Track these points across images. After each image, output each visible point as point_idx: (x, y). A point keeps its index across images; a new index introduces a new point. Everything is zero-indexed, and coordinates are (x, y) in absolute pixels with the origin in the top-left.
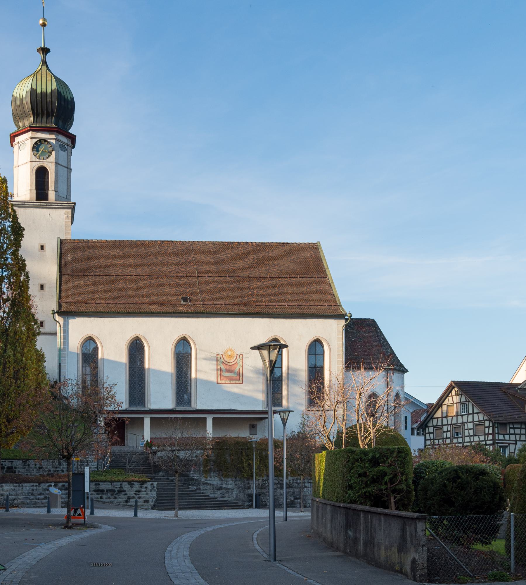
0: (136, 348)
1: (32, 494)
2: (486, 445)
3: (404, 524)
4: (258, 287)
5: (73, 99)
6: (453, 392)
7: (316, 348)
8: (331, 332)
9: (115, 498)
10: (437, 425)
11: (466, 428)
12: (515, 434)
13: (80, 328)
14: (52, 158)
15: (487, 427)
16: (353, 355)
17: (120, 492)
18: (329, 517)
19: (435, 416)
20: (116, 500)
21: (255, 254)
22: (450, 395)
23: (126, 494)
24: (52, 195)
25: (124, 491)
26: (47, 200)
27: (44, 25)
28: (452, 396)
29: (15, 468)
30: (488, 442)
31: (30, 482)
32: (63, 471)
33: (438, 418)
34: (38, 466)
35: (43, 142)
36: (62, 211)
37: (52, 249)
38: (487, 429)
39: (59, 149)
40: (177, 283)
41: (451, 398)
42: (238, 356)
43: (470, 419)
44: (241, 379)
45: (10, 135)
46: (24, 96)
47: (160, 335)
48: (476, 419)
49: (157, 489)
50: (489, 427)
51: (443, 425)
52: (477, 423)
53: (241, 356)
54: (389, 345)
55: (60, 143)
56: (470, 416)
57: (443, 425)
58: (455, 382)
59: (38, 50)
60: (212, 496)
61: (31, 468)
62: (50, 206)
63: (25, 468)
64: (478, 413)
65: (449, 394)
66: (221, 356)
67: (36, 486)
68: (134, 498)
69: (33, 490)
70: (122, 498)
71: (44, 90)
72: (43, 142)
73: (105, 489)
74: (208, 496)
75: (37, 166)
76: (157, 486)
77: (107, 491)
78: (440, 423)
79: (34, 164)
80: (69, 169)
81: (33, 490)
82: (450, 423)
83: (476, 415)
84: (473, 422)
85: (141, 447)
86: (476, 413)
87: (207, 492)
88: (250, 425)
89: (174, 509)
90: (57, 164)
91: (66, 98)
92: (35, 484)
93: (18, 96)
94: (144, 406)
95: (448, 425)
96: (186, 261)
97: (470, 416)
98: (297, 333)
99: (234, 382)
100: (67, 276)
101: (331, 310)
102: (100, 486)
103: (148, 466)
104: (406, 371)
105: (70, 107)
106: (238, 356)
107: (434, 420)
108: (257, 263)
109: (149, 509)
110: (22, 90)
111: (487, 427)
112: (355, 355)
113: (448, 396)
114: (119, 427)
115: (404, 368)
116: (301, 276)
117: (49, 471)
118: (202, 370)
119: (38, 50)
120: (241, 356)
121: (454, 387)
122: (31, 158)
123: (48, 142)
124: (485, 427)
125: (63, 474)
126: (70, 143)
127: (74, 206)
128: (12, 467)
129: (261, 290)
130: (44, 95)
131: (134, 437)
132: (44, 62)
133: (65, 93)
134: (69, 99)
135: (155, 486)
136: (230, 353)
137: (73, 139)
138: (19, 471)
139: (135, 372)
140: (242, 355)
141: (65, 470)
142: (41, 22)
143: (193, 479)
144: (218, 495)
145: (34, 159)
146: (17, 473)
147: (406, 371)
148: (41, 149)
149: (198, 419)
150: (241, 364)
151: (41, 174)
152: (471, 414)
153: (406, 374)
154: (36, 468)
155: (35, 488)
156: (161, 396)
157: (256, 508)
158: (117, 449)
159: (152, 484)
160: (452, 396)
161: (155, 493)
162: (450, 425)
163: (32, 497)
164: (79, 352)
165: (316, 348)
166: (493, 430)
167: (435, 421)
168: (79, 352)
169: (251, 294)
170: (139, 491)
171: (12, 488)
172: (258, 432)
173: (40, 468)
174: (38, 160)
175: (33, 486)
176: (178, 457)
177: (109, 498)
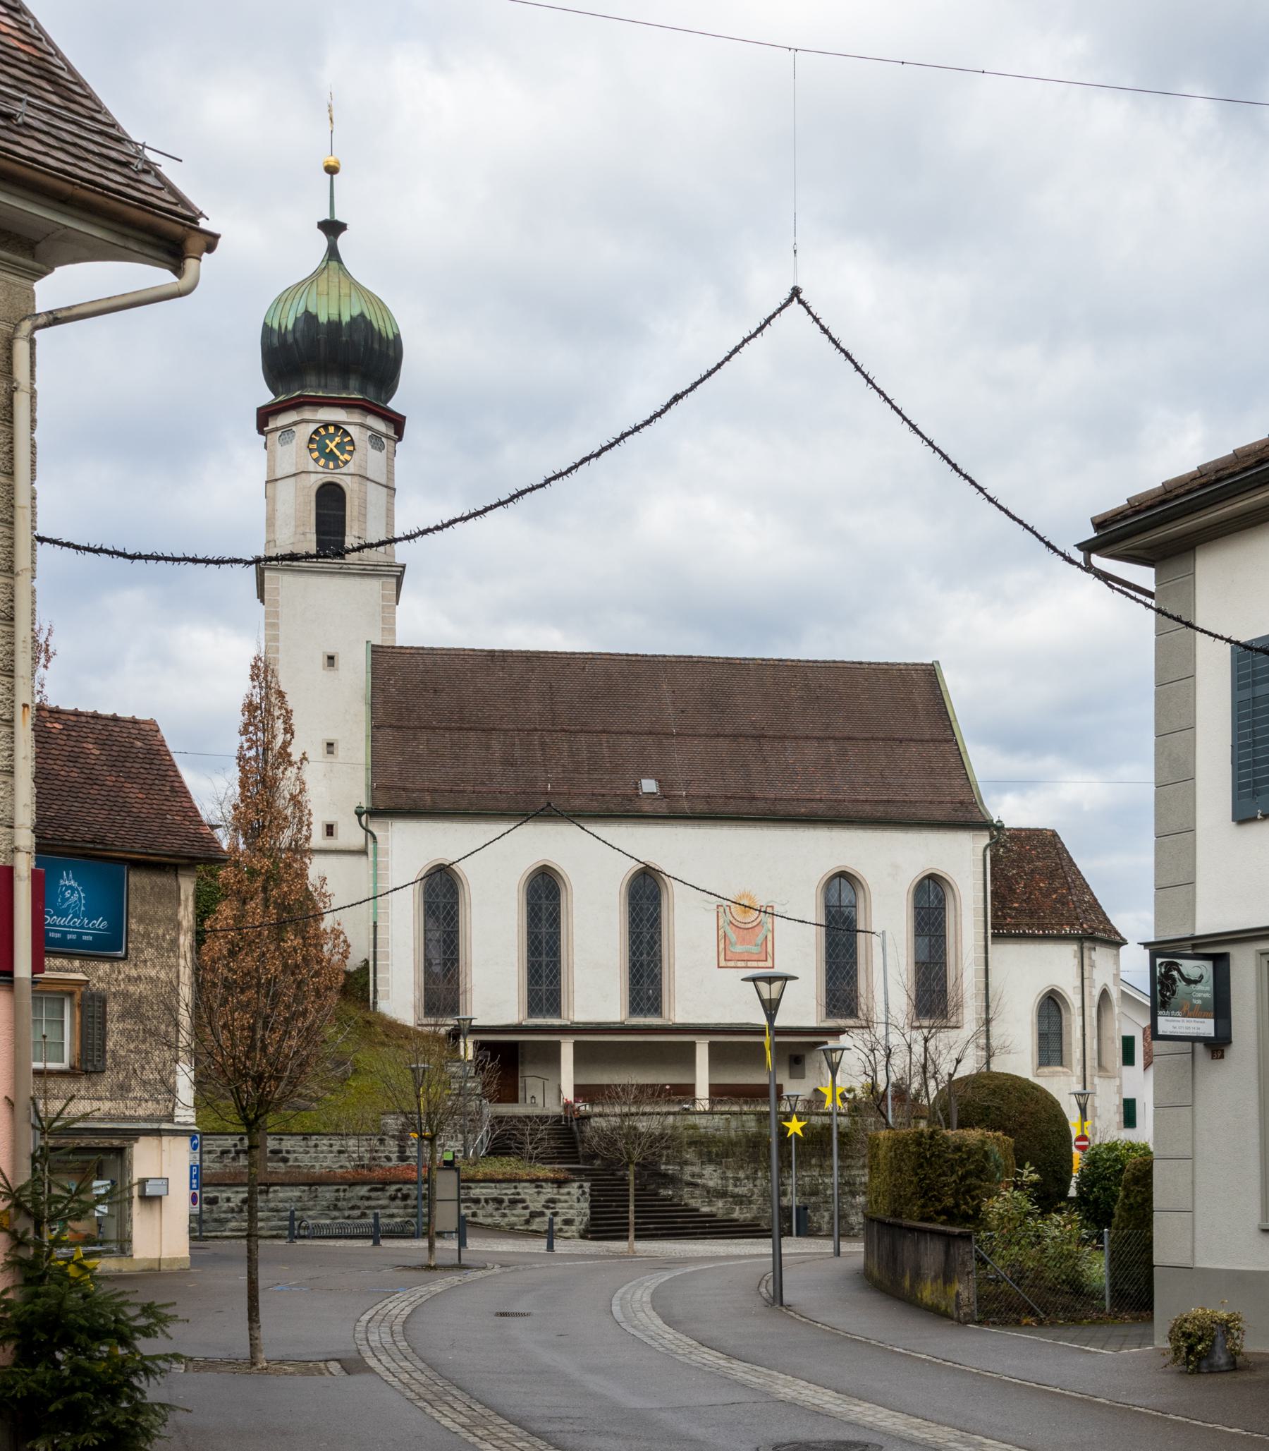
0: (544, 892)
1: (336, 1208)
3: (948, 1247)
5: (398, 336)
7: (931, 899)
8: (962, 860)
9: (504, 1215)
16: (1010, 908)
17: (513, 1202)
18: (876, 1241)
20: (506, 1219)
23: (526, 1208)
24: (778, 1039)
25: (523, 1201)
29: (288, 1152)
31: (328, 1184)
32: (389, 1159)
34: (335, 1148)
37: (355, 673)
39: (369, 447)
44: (770, 960)
46: (290, 327)
49: (591, 1195)
54: (1088, 886)
55: (370, 433)
60: (705, 1209)
61: (322, 1152)
63: (307, 1152)
67: (345, 1191)
68: (542, 1214)
69: (337, 1199)
70: (516, 1216)
71: (335, 317)
73: (482, 1197)
74: (697, 1210)
75: (320, 483)
76: (592, 1190)
77: (487, 1201)
80: (391, 489)
81: (337, 1199)
85: (553, 1109)
87: (694, 1203)
88: (791, 1056)
89: (626, 1238)
91: (384, 334)
92: (342, 1187)
93: (276, 326)
94: (559, 1016)
98: (889, 863)
101: (964, 815)
102: (472, 1192)
103: (566, 1141)
105: (391, 353)
109: (573, 1237)
112: (1015, 908)
114: (507, 1057)
115: (1119, 935)
117: (360, 1158)
118: (689, 930)
125: (390, 1164)
126: (391, 433)
127: (402, 573)
128: (280, 1152)
131: (540, 1082)
132: (333, 254)
133: (381, 323)
134: (391, 336)
135: (587, 1190)
137: (397, 423)
138: (296, 1160)
139: (540, 942)
141: (394, 1156)
143: (665, 1175)
144: (718, 1207)
146: (290, 1163)
149: (673, 1048)
153: (1123, 948)
154: (331, 1152)
155: (342, 1194)
157: (798, 1235)
158: (506, 1109)
159: (581, 1187)
161: (586, 1205)
163: (336, 1213)
170: (553, 1201)
171: (298, 1194)
172: (808, 1073)
173: (340, 1152)
174: (321, 469)
175: (338, 1191)
176: (635, 1128)
177: (491, 1215)
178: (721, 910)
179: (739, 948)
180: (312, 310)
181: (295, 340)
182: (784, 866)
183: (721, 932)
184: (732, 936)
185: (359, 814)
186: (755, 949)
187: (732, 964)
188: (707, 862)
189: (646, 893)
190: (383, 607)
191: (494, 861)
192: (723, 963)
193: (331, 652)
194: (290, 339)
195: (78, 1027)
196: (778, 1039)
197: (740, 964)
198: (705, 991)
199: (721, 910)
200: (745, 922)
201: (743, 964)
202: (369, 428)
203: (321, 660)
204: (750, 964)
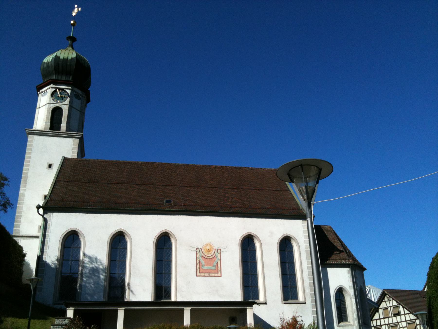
0: (118, 242)
6: (386, 299)
7: (286, 245)
8: (299, 231)
10: (377, 326)
11: (401, 326)
13: (62, 222)
15: (418, 325)
19: (374, 318)
21: (229, 173)
22: (384, 301)
24: (64, 126)
26: (60, 130)
28: (385, 301)
33: (376, 320)
36: (71, 140)
39: (74, 97)
41: (384, 303)
42: (216, 250)
43: (403, 319)
44: (219, 272)
45: (37, 87)
46: (50, 61)
47: (142, 230)
48: (408, 318)
51: (381, 325)
53: (219, 250)
56: (403, 317)
57: (381, 325)
58: (388, 290)
62: (61, 135)
64: (408, 314)
65: (383, 300)
66: (201, 250)
78: (379, 324)
79: (52, 105)
82: (387, 323)
83: (407, 316)
86: (407, 314)
95: (385, 325)
97: (403, 317)
98: (269, 231)
99: (213, 275)
100: (63, 182)
104: (365, 269)
106: (216, 250)
107: (373, 321)
111: (418, 325)
113: (382, 302)
116: (267, 189)
118: (183, 262)
119: (67, 40)
120: (219, 250)
121: (386, 294)
122: (50, 101)
123: (65, 91)
124: (417, 325)
130: (65, 60)
136: (208, 247)
140: (220, 249)
145: (52, 101)
147: (365, 269)
150: (219, 258)
151: (56, 114)
152: (403, 315)
153: (365, 272)
156: (140, 287)
160: (385, 301)
162: (388, 324)
165: (286, 245)
167: (374, 322)
174: (55, 103)
178: (198, 250)
179: (206, 268)
180: (58, 55)
181: (51, 64)
183: (198, 260)
184: (203, 262)
186: (213, 268)
187: (203, 274)
188: (192, 232)
189: (164, 243)
190: (73, 148)
192: (199, 274)
193: (50, 163)
194: (50, 64)
195: (107, 294)
196: (64, 126)
198: (187, 287)
199: (198, 250)
200: (208, 263)
202: (75, 92)
203: (46, 165)
204: (211, 274)
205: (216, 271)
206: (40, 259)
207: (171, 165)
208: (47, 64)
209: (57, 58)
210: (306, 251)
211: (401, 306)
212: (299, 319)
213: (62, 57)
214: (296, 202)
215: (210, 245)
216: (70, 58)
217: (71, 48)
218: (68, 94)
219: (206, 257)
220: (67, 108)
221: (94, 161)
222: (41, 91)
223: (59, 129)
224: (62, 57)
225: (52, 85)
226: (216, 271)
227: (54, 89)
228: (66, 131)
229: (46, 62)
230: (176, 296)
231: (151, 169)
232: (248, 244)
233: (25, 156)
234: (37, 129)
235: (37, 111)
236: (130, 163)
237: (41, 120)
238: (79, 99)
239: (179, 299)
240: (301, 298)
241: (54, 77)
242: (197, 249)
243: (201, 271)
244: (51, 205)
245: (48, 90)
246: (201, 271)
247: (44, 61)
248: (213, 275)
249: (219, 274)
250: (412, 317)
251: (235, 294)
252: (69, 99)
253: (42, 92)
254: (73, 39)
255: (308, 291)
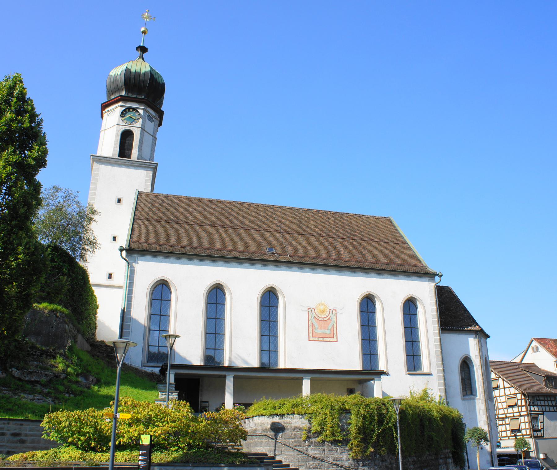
0: (216, 295)
2: (520, 416)
4: (343, 246)
7: (410, 306)
8: (425, 292)
12: (549, 406)
14: (139, 123)
27: (144, 32)
30: (522, 414)
35: (131, 110)
38: (519, 402)
39: (147, 119)
40: (260, 236)
42: (331, 311)
46: (119, 74)
48: (508, 392)
50: (521, 399)
52: (510, 396)
55: (147, 114)
59: (137, 49)
66: (313, 310)
71: (138, 70)
72: (131, 110)
80: (155, 139)
83: (507, 390)
84: (505, 395)
88: (348, 389)
90: (143, 129)
96: (268, 219)
97: (502, 391)
98: (391, 292)
99: (328, 339)
106: (331, 311)
108: (338, 227)
110: (118, 71)
119: (137, 49)
122: (119, 122)
124: (518, 400)
129: (346, 249)
130: (137, 74)
134: (161, 82)
136: (322, 308)
142: (143, 29)
145: (121, 123)
147: (488, 337)
148: (128, 116)
151: (126, 137)
164: (146, 325)
165: (410, 306)
166: (526, 402)
168: (146, 325)
169: (338, 252)
178: (310, 311)
179: (319, 331)
180: (129, 67)
182: (342, 290)
184: (316, 325)
185: (121, 250)
186: (328, 332)
187: (316, 339)
188: (302, 290)
189: (269, 299)
190: (146, 180)
191: (190, 280)
193: (119, 197)
194: (118, 78)
197: (320, 339)
200: (322, 327)
201: (321, 339)
202: (148, 112)
204: (325, 339)
205: (331, 336)
206: (125, 316)
207: (264, 206)
208: (116, 78)
209: (128, 71)
210: (432, 315)
211: (500, 380)
212: (429, 392)
213: (133, 70)
214: (418, 258)
215: (323, 304)
216: (143, 71)
217: (141, 60)
218: (140, 114)
219: (320, 319)
220: (139, 132)
221: (174, 197)
222: (107, 110)
223: (129, 156)
224: (133, 70)
225: (121, 103)
226: (331, 336)
227: (123, 109)
228: (138, 159)
229: (113, 75)
230: (285, 362)
231: (243, 210)
232: (368, 304)
233: (89, 188)
234: (103, 155)
235: (102, 134)
236: (216, 201)
237: (108, 145)
238: (152, 121)
239: (289, 366)
240: (425, 368)
241: (123, 93)
242: (308, 309)
243: (313, 336)
244: (134, 251)
245: (117, 109)
246: (313, 336)
247: (111, 74)
248: (328, 339)
249: (335, 339)
250: (513, 391)
251: (353, 362)
252: (141, 120)
253: (108, 111)
254: (143, 49)
255: (433, 360)
